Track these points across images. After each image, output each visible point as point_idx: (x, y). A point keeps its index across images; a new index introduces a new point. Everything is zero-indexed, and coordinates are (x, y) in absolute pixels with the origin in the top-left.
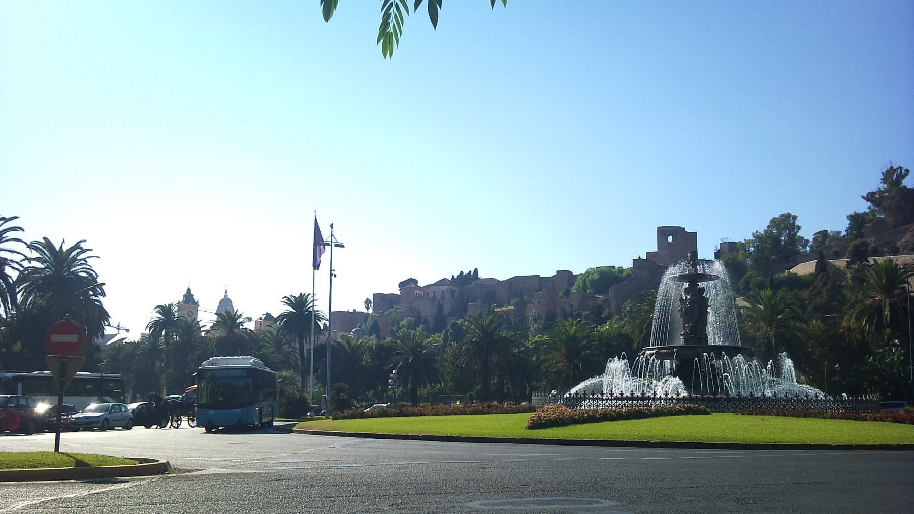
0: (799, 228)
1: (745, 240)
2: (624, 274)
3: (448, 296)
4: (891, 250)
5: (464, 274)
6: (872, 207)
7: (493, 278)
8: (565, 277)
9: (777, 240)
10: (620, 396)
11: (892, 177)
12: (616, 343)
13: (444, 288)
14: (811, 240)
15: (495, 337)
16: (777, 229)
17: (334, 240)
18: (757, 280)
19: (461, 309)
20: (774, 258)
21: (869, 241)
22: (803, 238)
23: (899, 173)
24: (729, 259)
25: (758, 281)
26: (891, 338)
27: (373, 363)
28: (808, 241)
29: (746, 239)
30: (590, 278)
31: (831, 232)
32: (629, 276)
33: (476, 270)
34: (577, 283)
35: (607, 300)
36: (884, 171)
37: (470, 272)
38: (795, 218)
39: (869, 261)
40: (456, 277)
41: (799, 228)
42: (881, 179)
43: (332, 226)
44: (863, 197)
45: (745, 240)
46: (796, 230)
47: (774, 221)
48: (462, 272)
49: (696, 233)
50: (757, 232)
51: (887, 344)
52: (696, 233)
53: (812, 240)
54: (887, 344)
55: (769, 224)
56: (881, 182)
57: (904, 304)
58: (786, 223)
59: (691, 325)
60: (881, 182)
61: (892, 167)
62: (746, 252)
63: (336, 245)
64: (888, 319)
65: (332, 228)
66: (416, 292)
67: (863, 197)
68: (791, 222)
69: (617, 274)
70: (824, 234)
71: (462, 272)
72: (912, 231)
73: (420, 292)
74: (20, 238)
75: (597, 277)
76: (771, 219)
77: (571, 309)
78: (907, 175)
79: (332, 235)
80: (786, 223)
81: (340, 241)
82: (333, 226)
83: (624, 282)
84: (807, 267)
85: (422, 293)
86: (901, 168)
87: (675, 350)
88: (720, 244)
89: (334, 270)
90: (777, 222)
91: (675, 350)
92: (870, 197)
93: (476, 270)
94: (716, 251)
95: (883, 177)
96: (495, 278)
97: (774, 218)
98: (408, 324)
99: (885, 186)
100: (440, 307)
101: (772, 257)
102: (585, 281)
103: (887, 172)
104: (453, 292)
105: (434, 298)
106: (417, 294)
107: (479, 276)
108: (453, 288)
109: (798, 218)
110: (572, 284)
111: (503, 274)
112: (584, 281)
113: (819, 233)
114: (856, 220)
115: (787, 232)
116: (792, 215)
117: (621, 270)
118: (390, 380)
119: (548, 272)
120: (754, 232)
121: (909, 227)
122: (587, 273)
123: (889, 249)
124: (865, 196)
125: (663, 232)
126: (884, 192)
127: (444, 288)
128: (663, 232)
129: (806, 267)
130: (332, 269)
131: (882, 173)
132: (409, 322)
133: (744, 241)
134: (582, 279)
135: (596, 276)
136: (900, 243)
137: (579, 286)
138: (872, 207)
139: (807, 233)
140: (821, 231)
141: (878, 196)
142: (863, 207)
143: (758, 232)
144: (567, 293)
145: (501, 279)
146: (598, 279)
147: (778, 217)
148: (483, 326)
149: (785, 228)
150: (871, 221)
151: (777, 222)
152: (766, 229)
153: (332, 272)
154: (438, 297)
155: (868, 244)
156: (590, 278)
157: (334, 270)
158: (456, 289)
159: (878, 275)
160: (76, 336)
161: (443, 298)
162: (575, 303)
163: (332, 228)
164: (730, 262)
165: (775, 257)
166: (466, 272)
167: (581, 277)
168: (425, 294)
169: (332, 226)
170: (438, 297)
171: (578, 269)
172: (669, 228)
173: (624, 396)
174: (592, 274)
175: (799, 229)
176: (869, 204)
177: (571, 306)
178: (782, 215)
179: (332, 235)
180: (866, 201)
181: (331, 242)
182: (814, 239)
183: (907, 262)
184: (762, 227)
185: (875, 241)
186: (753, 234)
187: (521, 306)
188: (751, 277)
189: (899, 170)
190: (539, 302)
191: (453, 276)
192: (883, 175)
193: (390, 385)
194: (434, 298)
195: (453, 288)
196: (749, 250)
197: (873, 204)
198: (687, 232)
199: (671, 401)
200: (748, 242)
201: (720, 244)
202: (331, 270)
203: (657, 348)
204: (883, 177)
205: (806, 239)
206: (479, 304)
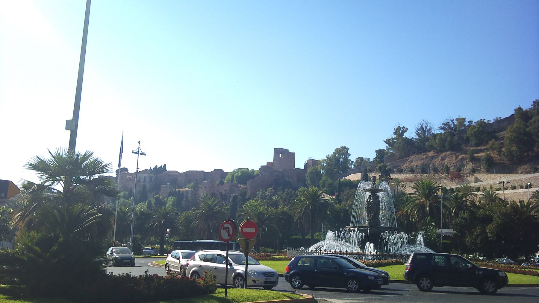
0: (350, 155)
1: (322, 159)
2: (255, 174)
3: (147, 180)
4: (399, 171)
5: (158, 167)
6: (388, 147)
7: (176, 171)
8: (219, 173)
9: (338, 160)
10: (375, 254)
11: (399, 132)
12: (281, 217)
13: (146, 175)
14: (355, 161)
15: (215, 210)
16: (339, 154)
17: (140, 151)
18: (329, 182)
19: (156, 188)
20: (336, 170)
21: (387, 164)
22: (350, 160)
23: (403, 129)
24: (314, 169)
25: (330, 183)
26: (431, 221)
27: (138, 223)
28: (353, 162)
29: (323, 159)
30: (236, 174)
31: (365, 158)
32: (258, 175)
33: (165, 165)
34: (227, 177)
35: (246, 188)
36: (395, 128)
37: (161, 166)
38: (348, 149)
39: (390, 176)
40: (152, 169)
41: (350, 155)
42: (394, 132)
43: (139, 142)
44: (384, 141)
45: (322, 159)
46: (348, 156)
47: (337, 150)
48: (156, 166)
49: (295, 153)
50: (328, 155)
51: (428, 224)
52: (295, 153)
53: (355, 162)
54: (428, 224)
55: (334, 151)
56: (393, 134)
57: (435, 204)
58: (343, 152)
59: (372, 215)
60: (393, 134)
61: (400, 126)
62: (322, 166)
63: (141, 154)
64: (428, 212)
65: (139, 143)
66: (128, 176)
67: (384, 141)
68: (346, 151)
69: (251, 173)
70: (361, 159)
71: (156, 166)
72: (409, 161)
73: (130, 177)
74: (49, 153)
75: (240, 174)
76: (336, 148)
77: (225, 192)
78: (407, 131)
79: (139, 148)
80: (343, 152)
81: (143, 151)
82: (140, 142)
83: (255, 178)
84: (355, 176)
85: (132, 177)
86: (404, 127)
87: (368, 228)
88: (308, 160)
89: (139, 169)
90: (339, 150)
91: (368, 228)
92: (388, 141)
93: (165, 165)
94: (305, 164)
95: (394, 131)
96: (177, 171)
97: (337, 149)
98: (123, 196)
99: (395, 136)
100: (145, 187)
101: (335, 170)
102: (233, 176)
103: (397, 129)
104: (151, 178)
105: (139, 181)
106: (128, 177)
107: (166, 169)
108: (151, 175)
109: (349, 149)
110: (225, 178)
111: (182, 169)
112: (232, 176)
113: (358, 158)
114: (380, 153)
115: (344, 156)
116: (347, 147)
117: (253, 171)
118: (167, 235)
119: (209, 169)
120: (327, 155)
121: (408, 159)
122: (234, 172)
123: (397, 170)
124: (385, 140)
125: (277, 151)
126: (395, 139)
127: (146, 175)
128: (277, 151)
129: (354, 176)
130: (138, 168)
131: (394, 129)
132: (125, 195)
133: (321, 160)
134: (231, 175)
135: (239, 174)
136: (403, 167)
137: (229, 179)
138: (388, 147)
139: (353, 158)
140: (360, 157)
141: (391, 141)
142: (384, 146)
143: (329, 155)
144: (222, 183)
145: (180, 172)
146: (241, 176)
147: (339, 148)
148: (209, 204)
149: (342, 154)
150: (387, 154)
151: (339, 150)
152: (333, 154)
153: (138, 170)
154: (142, 180)
155: (386, 166)
156: (236, 174)
157: (139, 169)
158: (153, 176)
159: (423, 188)
160: (244, 231)
161: (145, 181)
162: (227, 188)
163: (139, 143)
164: (314, 171)
165: (336, 169)
166: (159, 166)
167: (230, 174)
168: (133, 178)
169: (139, 142)
170: (142, 180)
171: (229, 167)
172: (280, 149)
173: (337, 252)
174: (237, 173)
175: (350, 155)
176: (387, 145)
177: (226, 191)
178: (342, 147)
179: (139, 148)
180: (385, 143)
181: (139, 152)
182: (356, 161)
183: (407, 178)
184: (330, 152)
185: (390, 165)
186: (326, 156)
187: (196, 188)
188: (326, 180)
189: (403, 128)
190: (205, 187)
191: (151, 168)
192: (395, 130)
193: (167, 238)
194: (139, 181)
195: (151, 175)
196: (324, 165)
197: (389, 145)
198: (290, 152)
199: (379, 257)
200: (323, 160)
201: (308, 160)
202: (137, 168)
203: (358, 227)
204: (394, 131)
205: (352, 161)
206: (168, 186)
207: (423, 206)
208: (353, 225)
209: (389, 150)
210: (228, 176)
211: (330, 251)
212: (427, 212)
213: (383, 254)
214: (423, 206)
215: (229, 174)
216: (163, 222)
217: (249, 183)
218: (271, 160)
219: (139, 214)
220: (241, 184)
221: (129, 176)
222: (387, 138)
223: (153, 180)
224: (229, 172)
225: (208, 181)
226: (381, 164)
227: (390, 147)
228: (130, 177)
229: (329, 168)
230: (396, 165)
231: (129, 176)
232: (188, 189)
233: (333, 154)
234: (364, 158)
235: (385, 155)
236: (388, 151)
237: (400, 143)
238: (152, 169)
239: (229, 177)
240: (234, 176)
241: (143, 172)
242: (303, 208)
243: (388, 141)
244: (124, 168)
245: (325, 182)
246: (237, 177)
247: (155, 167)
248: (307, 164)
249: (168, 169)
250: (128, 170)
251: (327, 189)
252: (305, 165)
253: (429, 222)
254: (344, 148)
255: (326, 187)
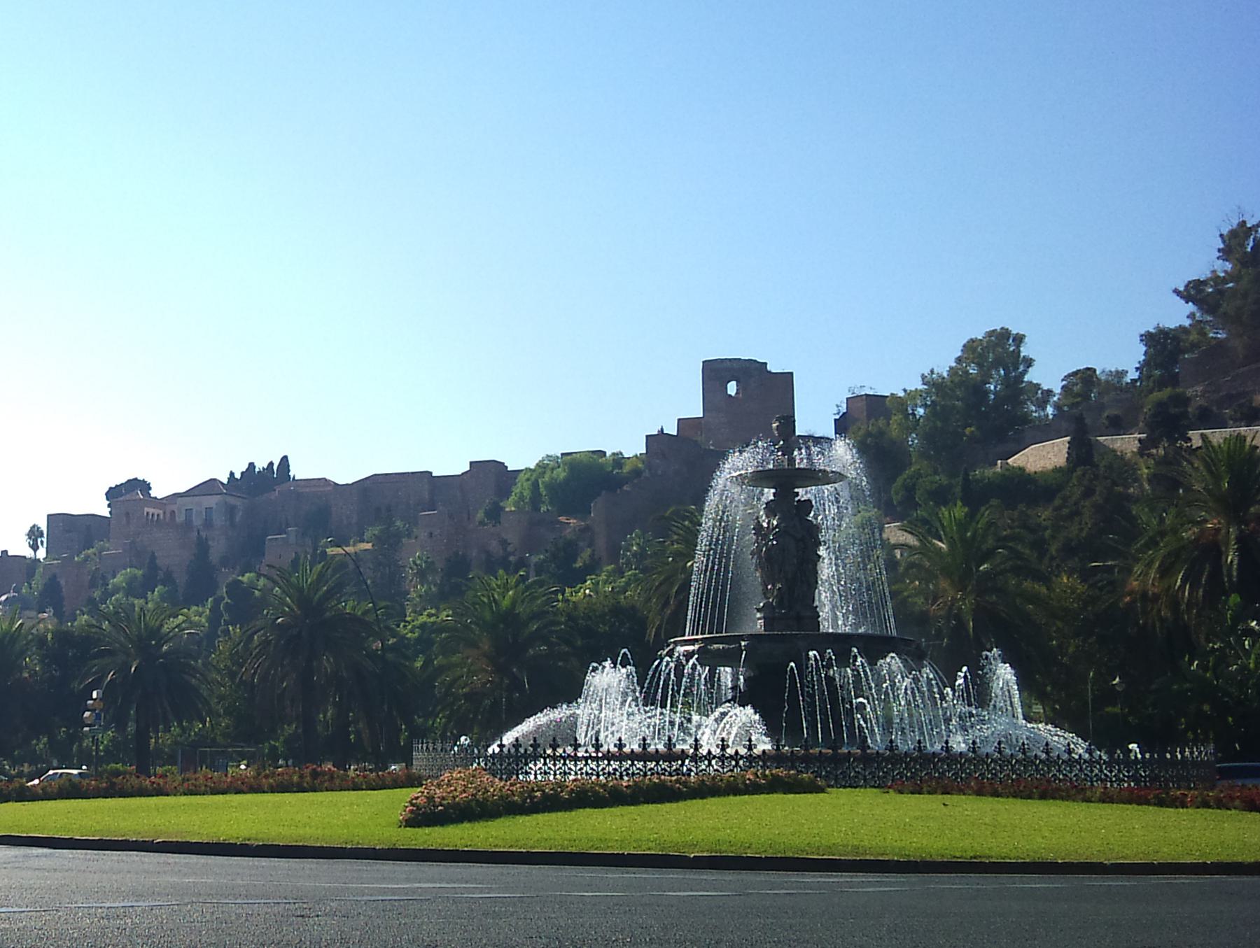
0: (1029, 362)
1: (905, 390)
2: (626, 469)
3: (219, 520)
5: (257, 470)
7: (325, 479)
9: (977, 390)
16: (980, 365)
18: (932, 482)
21: (1190, 392)
28: (1049, 393)
29: (908, 389)
30: (547, 478)
32: (637, 473)
33: (285, 460)
34: (516, 490)
35: (587, 529)
36: (1225, 232)
37: (271, 464)
38: (1019, 339)
39: (1190, 440)
40: (238, 476)
41: (1029, 362)
42: (1219, 250)
44: (1176, 292)
45: (905, 390)
46: (1021, 368)
47: (971, 347)
48: (252, 465)
50: (932, 372)
61: (1244, 222)
64: (1235, 574)
67: (1176, 292)
68: (1011, 349)
70: (1086, 376)
71: (252, 465)
73: (156, 511)
77: (505, 549)
83: (625, 488)
85: (161, 512)
87: (743, 643)
88: (847, 399)
91: (743, 643)
92: (1193, 292)
93: (285, 460)
94: (837, 417)
95: (1222, 246)
96: (328, 478)
97: (972, 341)
99: (1228, 266)
100: (203, 547)
101: (968, 430)
102: (535, 485)
103: (1233, 233)
104: (231, 510)
106: (148, 513)
108: (231, 500)
109: (1026, 340)
110: (507, 494)
115: (1002, 372)
116: (1014, 332)
117: (618, 459)
118: (87, 714)
119: (451, 464)
122: (541, 466)
124: (1182, 289)
126: (1225, 280)
127: (212, 501)
128: (715, 372)
129: (1044, 453)
131: (1221, 235)
132: (131, 581)
133: (901, 394)
134: (528, 480)
135: (561, 474)
137: (522, 498)
140: (1079, 371)
141: (1210, 290)
142: (1178, 315)
143: (936, 371)
144: (495, 513)
145: (341, 481)
146: (567, 481)
147: (980, 338)
148: (301, 590)
149: (997, 363)
150: (1194, 346)
152: (954, 365)
156: (547, 478)
158: (238, 503)
161: (208, 524)
166: (261, 465)
168: (168, 515)
174: (553, 469)
176: (1191, 307)
178: (991, 333)
182: (1063, 387)
184: (943, 360)
185: (1204, 392)
186: (923, 377)
187: (389, 542)
188: (918, 475)
190: (431, 535)
191: (232, 474)
192: (1224, 242)
194: (188, 524)
195: (231, 500)
196: (914, 415)
197: (1200, 308)
198: (770, 372)
200: (911, 395)
201: (847, 399)
203: (702, 639)
204: (1222, 246)
205: (1045, 388)
206: (292, 539)
207: (1211, 550)
208: (702, 634)
209: (1202, 328)
210: (519, 485)
211: (597, 746)
212: (1230, 576)
213: (778, 749)
214: (1211, 550)
215: (522, 477)
216: (133, 669)
217: (597, 509)
218: (696, 411)
219: (53, 644)
220: (568, 513)
221: (151, 510)
222: (1190, 279)
223: (238, 519)
224: (522, 471)
225: (441, 508)
226: (1167, 392)
227: (1209, 318)
228: (156, 511)
229: (939, 424)
230: (1234, 392)
231: (151, 510)
232: (370, 544)
233: (954, 365)
234: (1098, 372)
235: (1184, 352)
236: (1203, 333)
237: (1245, 295)
238: (238, 476)
239: (521, 488)
240: (541, 485)
241: (196, 493)
242: (672, 584)
243: (1193, 292)
244: (136, 479)
245: (914, 485)
246: (551, 487)
247: (247, 467)
248: (844, 414)
249: (299, 471)
250: (150, 489)
251: (924, 514)
252: (835, 420)
253: (1237, 619)
254: (1004, 335)
255: (920, 506)
